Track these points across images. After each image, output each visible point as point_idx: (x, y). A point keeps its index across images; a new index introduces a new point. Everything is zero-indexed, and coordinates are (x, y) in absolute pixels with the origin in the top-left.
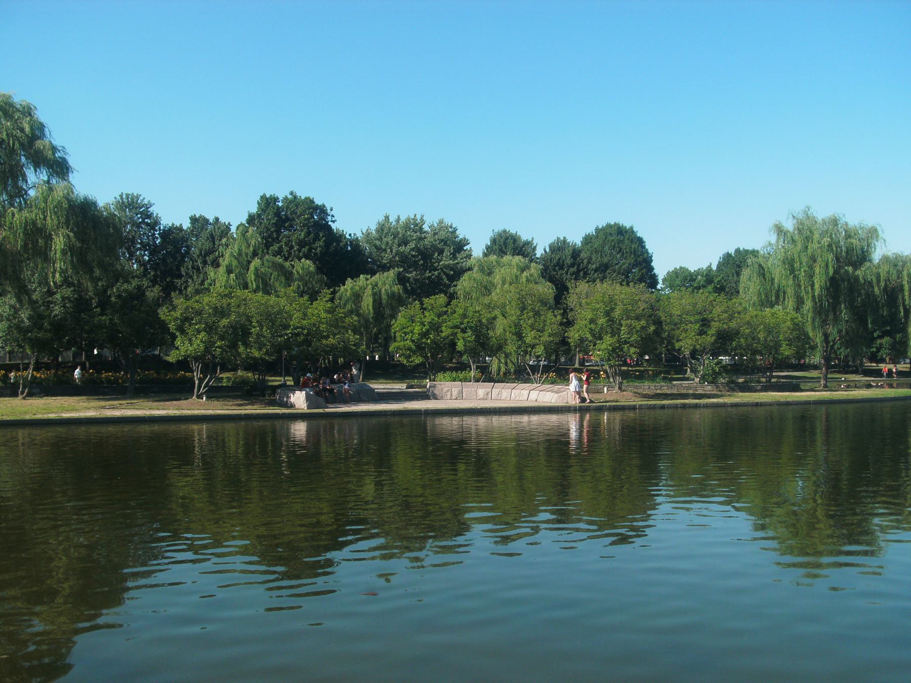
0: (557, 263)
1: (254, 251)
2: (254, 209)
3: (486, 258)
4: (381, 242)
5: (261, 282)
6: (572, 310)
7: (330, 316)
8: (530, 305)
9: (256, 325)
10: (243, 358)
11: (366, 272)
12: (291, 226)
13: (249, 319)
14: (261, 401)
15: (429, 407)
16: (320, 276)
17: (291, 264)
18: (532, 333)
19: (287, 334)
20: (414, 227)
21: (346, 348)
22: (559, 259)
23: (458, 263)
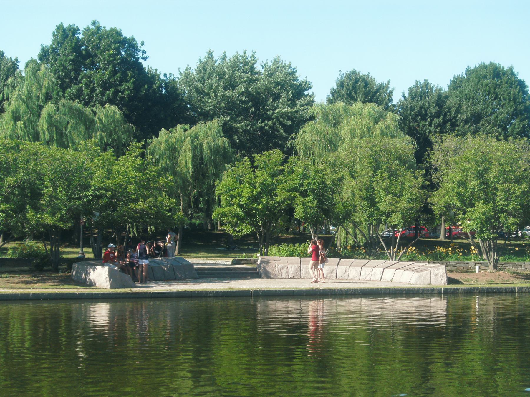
0: (419, 112)
1: (47, 93)
2: (48, 42)
4: (203, 84)
5: (55, 132)
6: (436, 170)
7: (140, 174)
8: (385, 164)
9: (49, 184)
10: (32, 226)
12: (93, 63)
13: (40, 177)
15: (239, 287)
16: (127, 125)
17: (92, 110)
18: (387, 198)
19: (86, 197)
20: (243, 66)
23: (297, 111)
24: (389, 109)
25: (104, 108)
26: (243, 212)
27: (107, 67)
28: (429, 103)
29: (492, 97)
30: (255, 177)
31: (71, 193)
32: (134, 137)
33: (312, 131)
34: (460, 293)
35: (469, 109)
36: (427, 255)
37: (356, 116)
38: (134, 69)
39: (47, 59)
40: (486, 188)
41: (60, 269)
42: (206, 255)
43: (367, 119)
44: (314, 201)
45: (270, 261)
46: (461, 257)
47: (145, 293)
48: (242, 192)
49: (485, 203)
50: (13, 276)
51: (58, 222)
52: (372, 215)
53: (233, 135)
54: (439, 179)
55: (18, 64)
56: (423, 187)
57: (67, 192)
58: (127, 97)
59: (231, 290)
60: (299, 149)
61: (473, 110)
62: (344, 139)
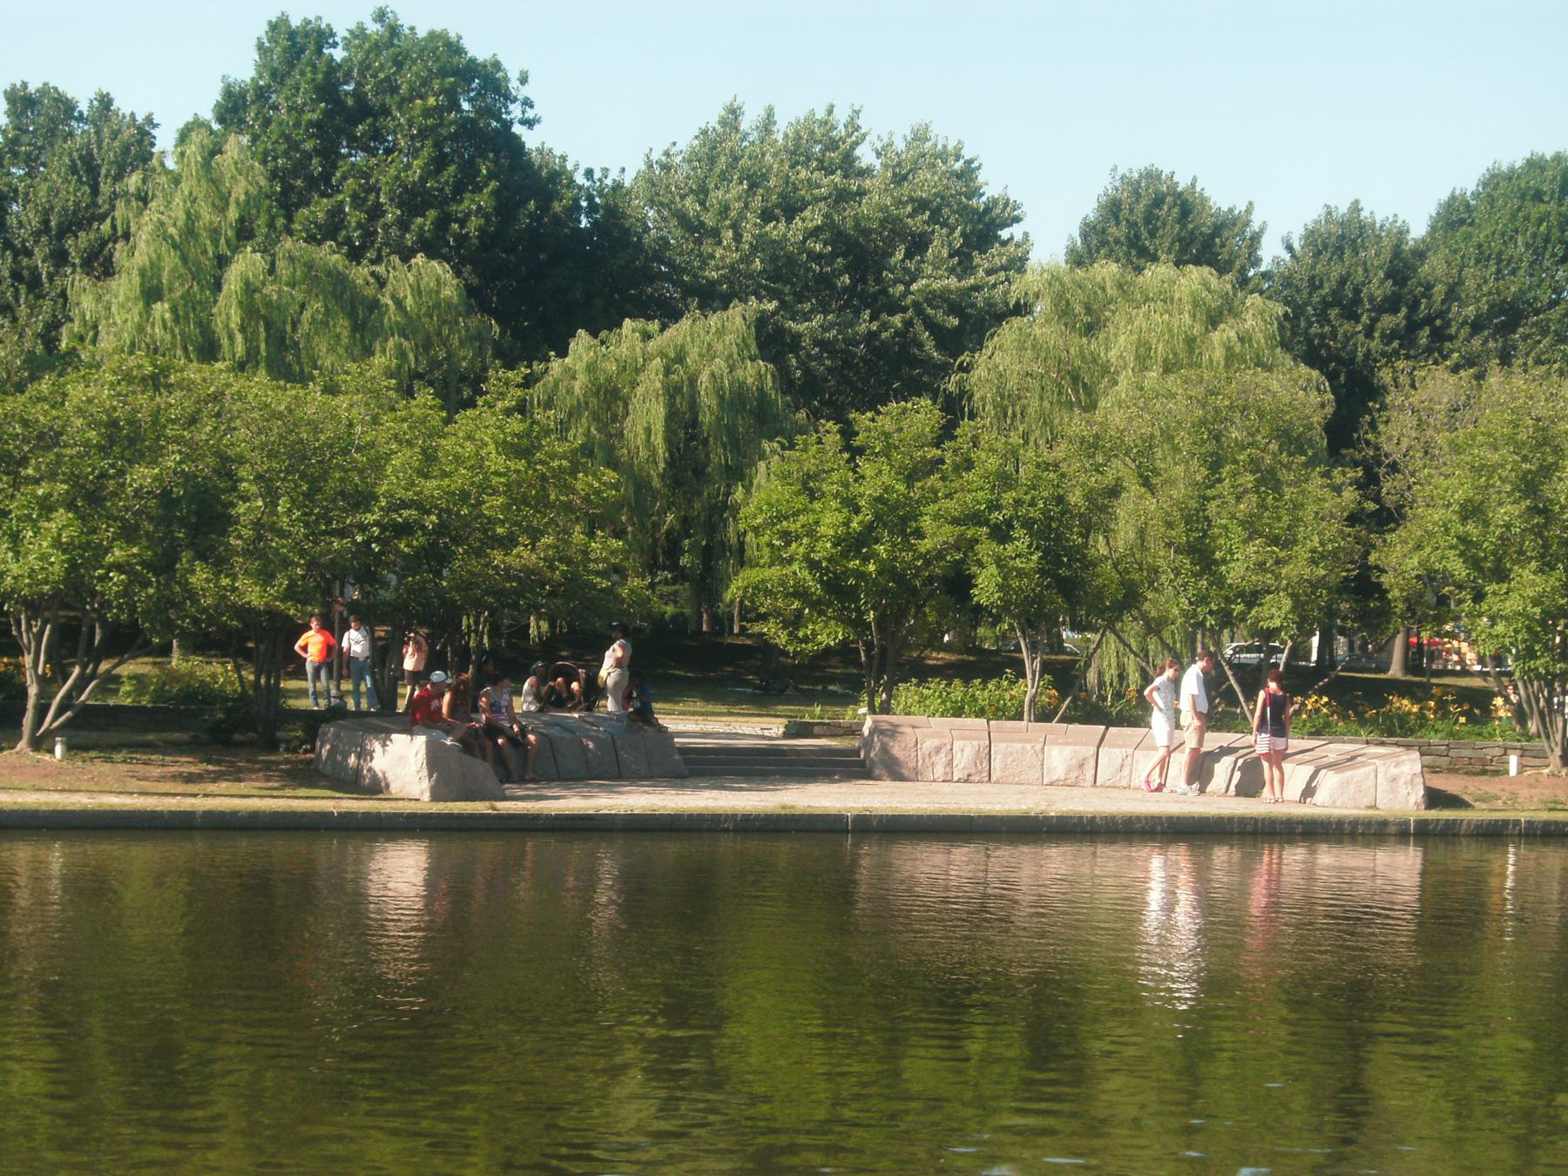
0: (1334, 293)
1: (241, 220)
2: (244, 69)
3: (1080, 273)
4: (702, 204)
5: (263, 335)
6: (1394, 468)
7: (521, 465)
8: (1244, 448)
9: (254, 489)
10: (205, 611)
11: (642, 310)
12: (377, 135)
13: (226, 467)
14: (268, 766)
15: (813, 804)
16: (474, 321)
17: (373, 274)
18: (1251, 549)
19: (363, 528)
20: (823, 151)
21: (574, 586)
22: (1342, 281)
23: (976, 288)
24: (1250, 286)
25: (410, 268)
26: (821, 581)
27: (418, 145)
28: (1366, 270)
29: (1556, 255)
30: (856, 480)
31: (319, 517)
32: (495, 356)
33: (1022, 348)
34: (1465, 836)
35: (1485, 289)
36: (1363, 722)
37: (1152, 305)
38: (497, 153)
39: (242, 121)
40: (1545, 525)
41: (280, 741)
42: (699, 706)
43: (1187, 316)
44: (1032, 554)
45: (901, 730)
46: (1464, 728)
47: (536, 817)
48: (817, 523)
49: (1542, 571)
50: (145, 757)
51: (282, 601)
52: (1203, 600)
53: (786, 354)
54: (1402, 496)
55: (154, 132)
56: (1352, 519)
57: (305, 514)
58: (478, 237)
59: (787, 812)
60: (983, 399)
61: (1498, 294)
62: (1117, 373)
